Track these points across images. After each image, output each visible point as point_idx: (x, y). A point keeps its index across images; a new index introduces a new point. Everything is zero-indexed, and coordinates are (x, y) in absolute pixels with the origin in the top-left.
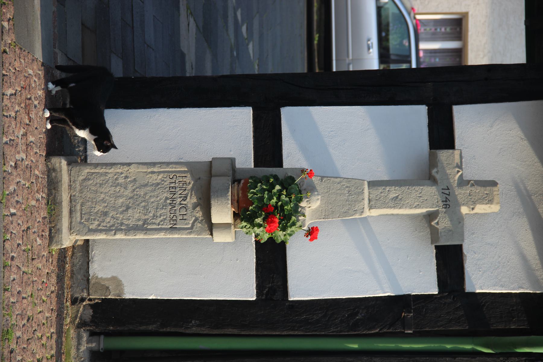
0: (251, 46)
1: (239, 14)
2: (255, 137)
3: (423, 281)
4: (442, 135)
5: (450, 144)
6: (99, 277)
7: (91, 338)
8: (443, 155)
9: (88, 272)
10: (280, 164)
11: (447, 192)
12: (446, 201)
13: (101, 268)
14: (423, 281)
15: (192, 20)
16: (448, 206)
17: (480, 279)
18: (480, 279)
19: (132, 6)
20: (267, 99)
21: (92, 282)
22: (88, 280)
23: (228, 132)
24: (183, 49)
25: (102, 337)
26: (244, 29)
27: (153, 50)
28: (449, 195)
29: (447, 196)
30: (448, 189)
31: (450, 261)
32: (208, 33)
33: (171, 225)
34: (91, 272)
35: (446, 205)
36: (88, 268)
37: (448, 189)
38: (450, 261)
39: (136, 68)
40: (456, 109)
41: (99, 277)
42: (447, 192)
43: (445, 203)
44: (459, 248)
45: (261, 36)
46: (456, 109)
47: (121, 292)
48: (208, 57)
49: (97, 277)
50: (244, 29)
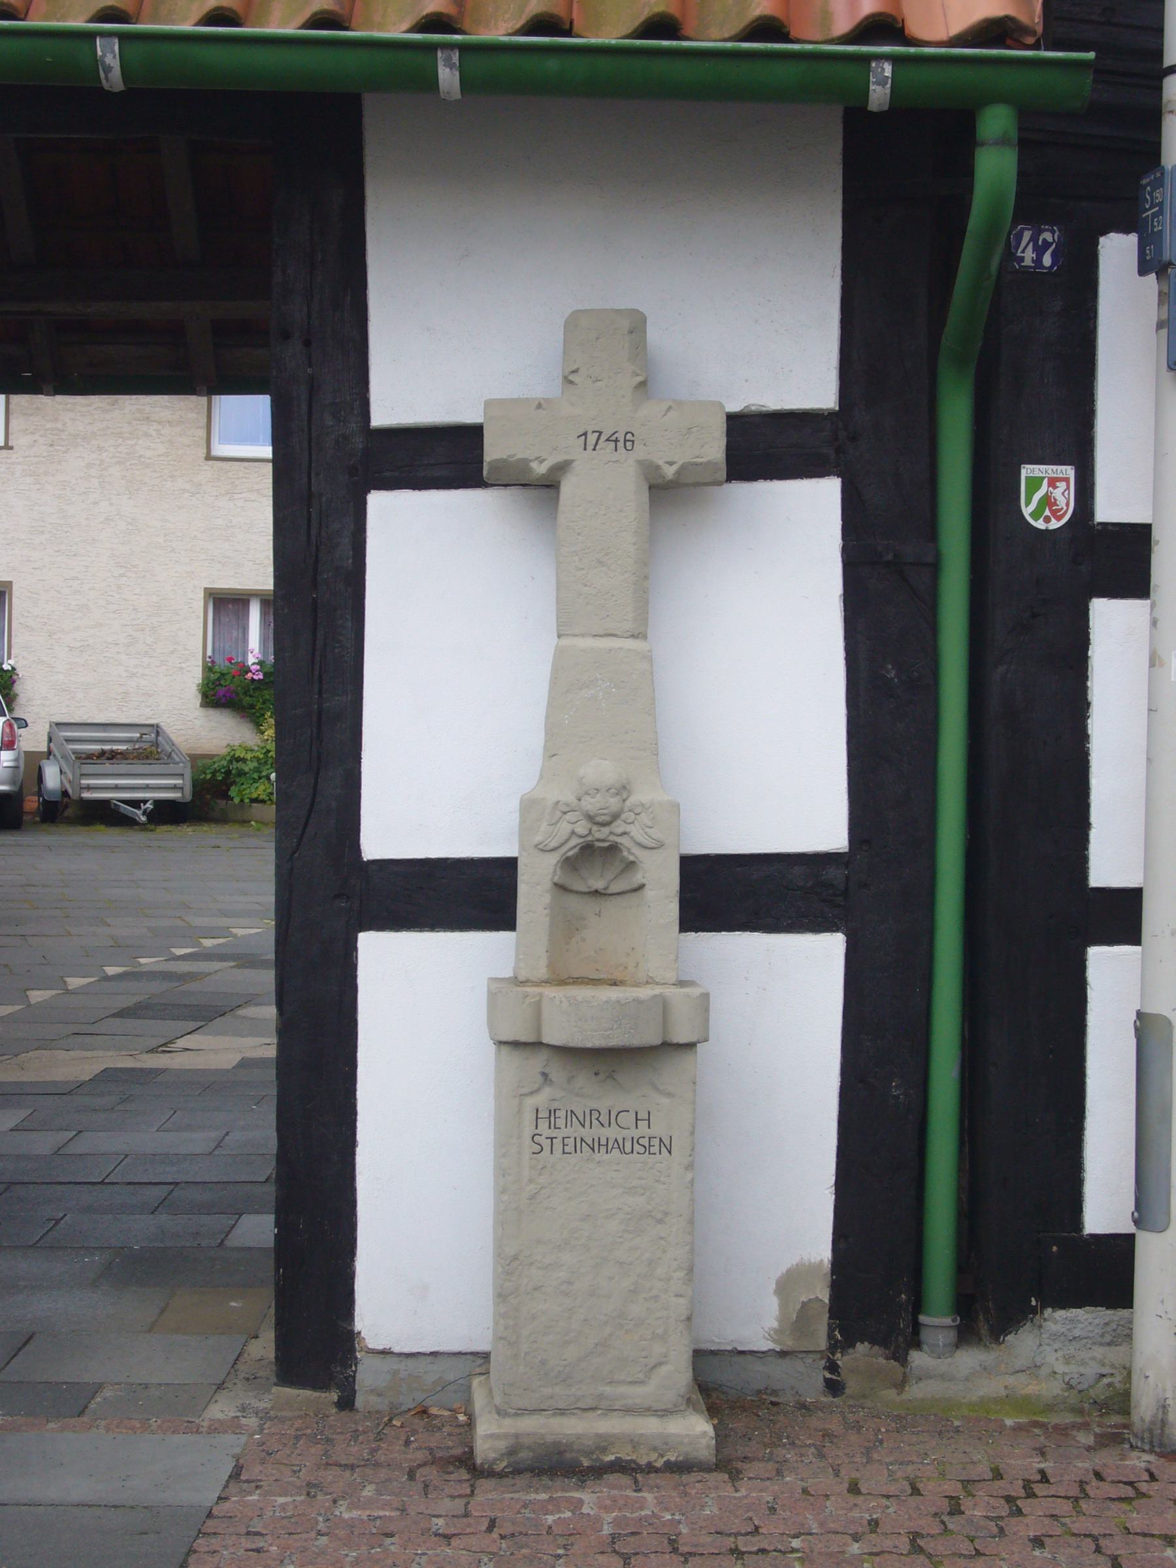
0: (239, 932)
1: (111, 971)
2: (844, 1017)
3: (813, 507)
4: (446, 457)
5: (471, 435)
6: (775, 1324)
7: (925, 1347)
8: (493, 450)
9: (763, 1352)
10: (509, 865)
11: (592, 438)
12: (616, 441)
13: (754, 1317)
14: (813, 507)
15: (181, 1043)
16: (629, 437)
17: (804, 375)
18: (804, 375)
19: (129, 1183)
20: (339, 895)
21: (789, 1344)
22: (783, 1354)
23: (420, 1002)
24: (235, 1063)
25: (922, 1319)
26: (208, 943)
27: (227, 1134)
28: (600, 433)
29: (603, 438)
30: (585, 434)
31: (764, 447)
32: (207, 1013)
33: (664, 1149)
34: (765, 1345)
35: (625, 441)
36: (752, 1352)
37: (585, 434)
38: (764, 447)
39: (263, 1179)
40: (380, 417)
41: (775, 1324)
42: (592, 438)
43: (621, 444)
44: (731, 418)
45: (226, 914)
46: (380, 417)
47: (814, 1268)
48: (250, 1011)
49: (776, 1331)
50: (208, 943)
